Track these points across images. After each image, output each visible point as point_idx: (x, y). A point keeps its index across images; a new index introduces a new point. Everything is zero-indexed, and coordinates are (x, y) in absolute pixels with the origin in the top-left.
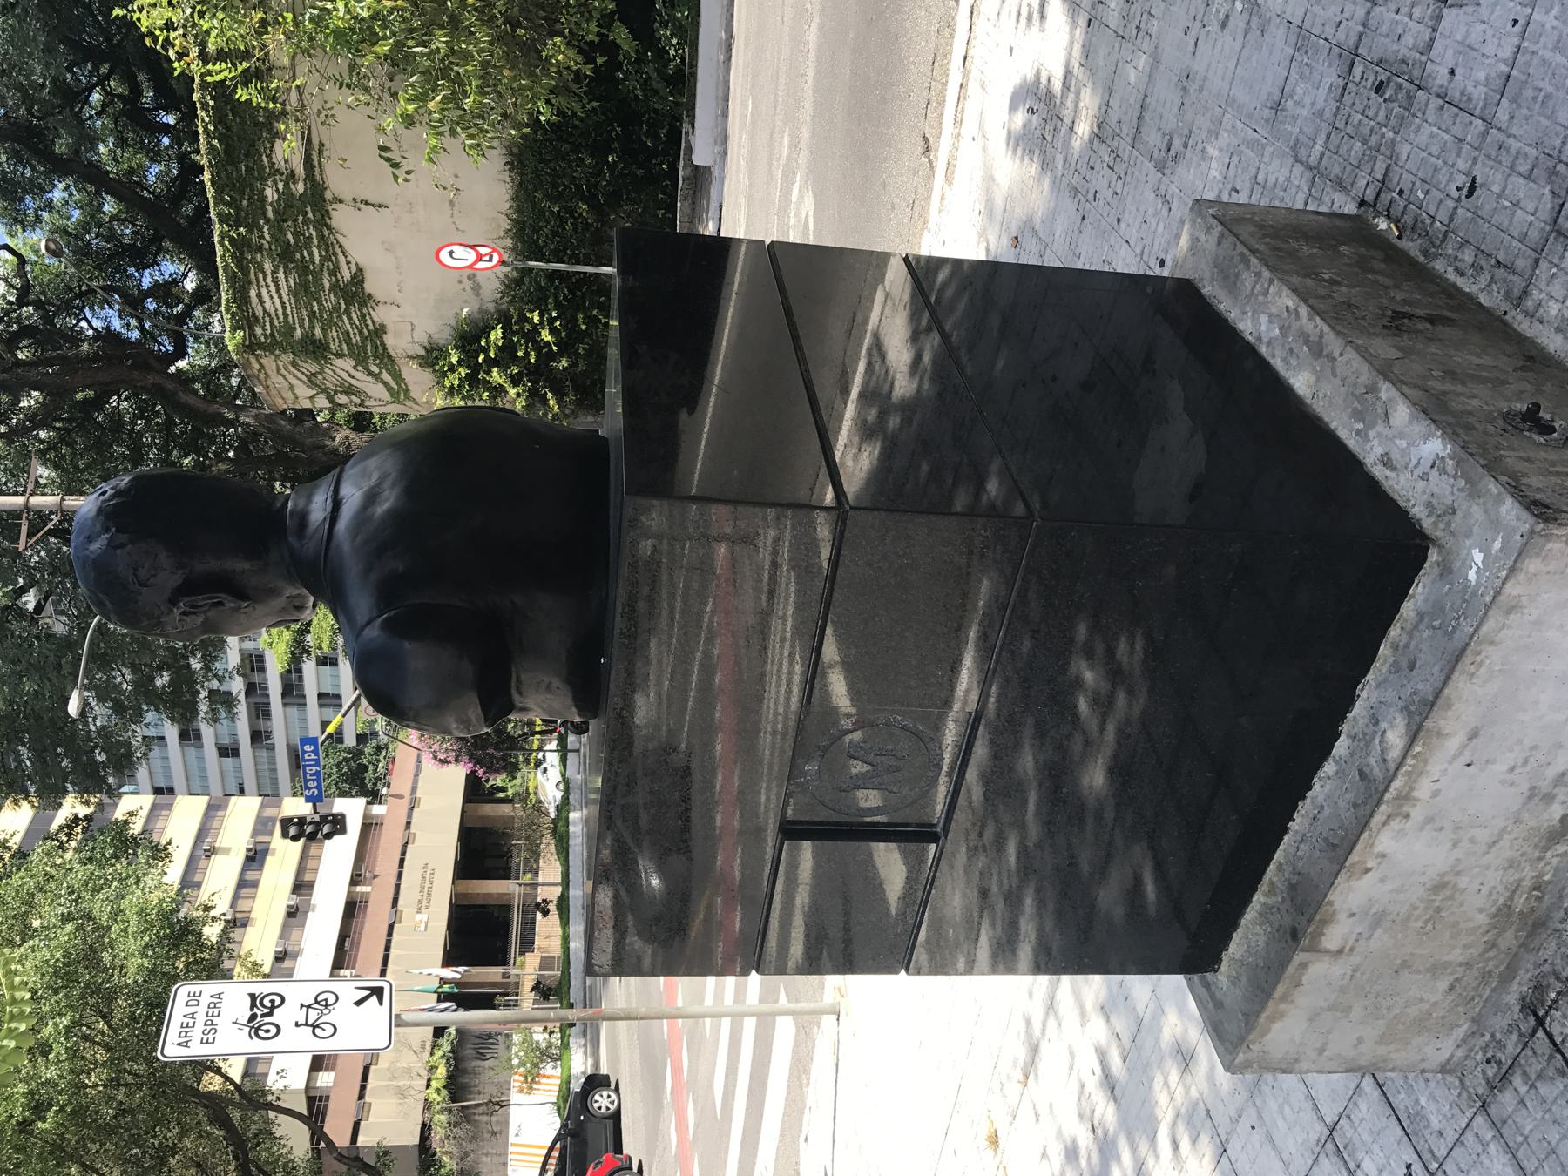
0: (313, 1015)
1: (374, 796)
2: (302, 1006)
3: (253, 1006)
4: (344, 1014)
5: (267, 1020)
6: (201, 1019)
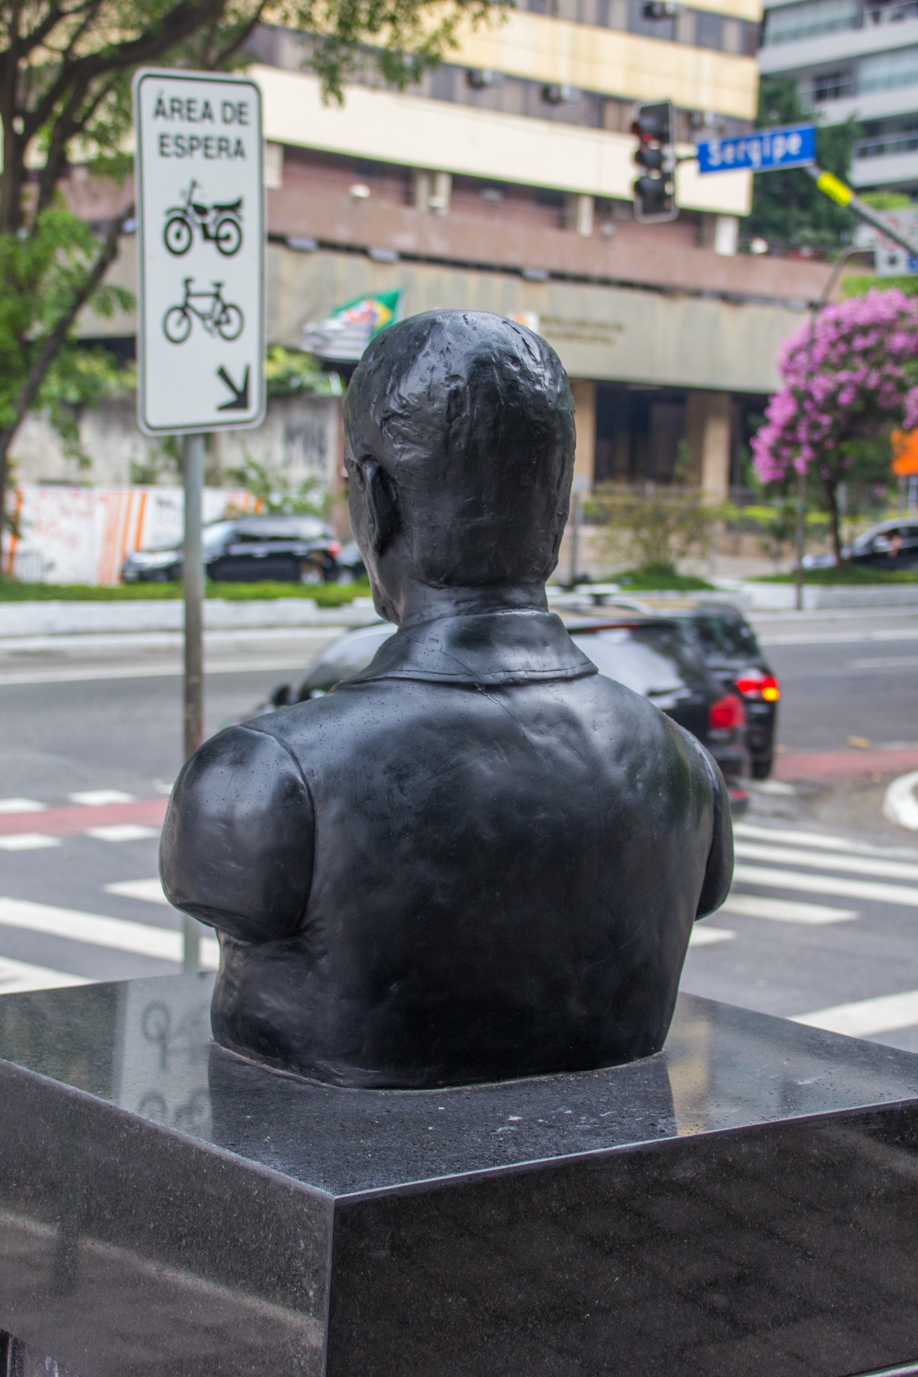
0: (203, 305)
2: (218, 285)
3: (220, 208)
5: (198, 234)
6: (202, 129)
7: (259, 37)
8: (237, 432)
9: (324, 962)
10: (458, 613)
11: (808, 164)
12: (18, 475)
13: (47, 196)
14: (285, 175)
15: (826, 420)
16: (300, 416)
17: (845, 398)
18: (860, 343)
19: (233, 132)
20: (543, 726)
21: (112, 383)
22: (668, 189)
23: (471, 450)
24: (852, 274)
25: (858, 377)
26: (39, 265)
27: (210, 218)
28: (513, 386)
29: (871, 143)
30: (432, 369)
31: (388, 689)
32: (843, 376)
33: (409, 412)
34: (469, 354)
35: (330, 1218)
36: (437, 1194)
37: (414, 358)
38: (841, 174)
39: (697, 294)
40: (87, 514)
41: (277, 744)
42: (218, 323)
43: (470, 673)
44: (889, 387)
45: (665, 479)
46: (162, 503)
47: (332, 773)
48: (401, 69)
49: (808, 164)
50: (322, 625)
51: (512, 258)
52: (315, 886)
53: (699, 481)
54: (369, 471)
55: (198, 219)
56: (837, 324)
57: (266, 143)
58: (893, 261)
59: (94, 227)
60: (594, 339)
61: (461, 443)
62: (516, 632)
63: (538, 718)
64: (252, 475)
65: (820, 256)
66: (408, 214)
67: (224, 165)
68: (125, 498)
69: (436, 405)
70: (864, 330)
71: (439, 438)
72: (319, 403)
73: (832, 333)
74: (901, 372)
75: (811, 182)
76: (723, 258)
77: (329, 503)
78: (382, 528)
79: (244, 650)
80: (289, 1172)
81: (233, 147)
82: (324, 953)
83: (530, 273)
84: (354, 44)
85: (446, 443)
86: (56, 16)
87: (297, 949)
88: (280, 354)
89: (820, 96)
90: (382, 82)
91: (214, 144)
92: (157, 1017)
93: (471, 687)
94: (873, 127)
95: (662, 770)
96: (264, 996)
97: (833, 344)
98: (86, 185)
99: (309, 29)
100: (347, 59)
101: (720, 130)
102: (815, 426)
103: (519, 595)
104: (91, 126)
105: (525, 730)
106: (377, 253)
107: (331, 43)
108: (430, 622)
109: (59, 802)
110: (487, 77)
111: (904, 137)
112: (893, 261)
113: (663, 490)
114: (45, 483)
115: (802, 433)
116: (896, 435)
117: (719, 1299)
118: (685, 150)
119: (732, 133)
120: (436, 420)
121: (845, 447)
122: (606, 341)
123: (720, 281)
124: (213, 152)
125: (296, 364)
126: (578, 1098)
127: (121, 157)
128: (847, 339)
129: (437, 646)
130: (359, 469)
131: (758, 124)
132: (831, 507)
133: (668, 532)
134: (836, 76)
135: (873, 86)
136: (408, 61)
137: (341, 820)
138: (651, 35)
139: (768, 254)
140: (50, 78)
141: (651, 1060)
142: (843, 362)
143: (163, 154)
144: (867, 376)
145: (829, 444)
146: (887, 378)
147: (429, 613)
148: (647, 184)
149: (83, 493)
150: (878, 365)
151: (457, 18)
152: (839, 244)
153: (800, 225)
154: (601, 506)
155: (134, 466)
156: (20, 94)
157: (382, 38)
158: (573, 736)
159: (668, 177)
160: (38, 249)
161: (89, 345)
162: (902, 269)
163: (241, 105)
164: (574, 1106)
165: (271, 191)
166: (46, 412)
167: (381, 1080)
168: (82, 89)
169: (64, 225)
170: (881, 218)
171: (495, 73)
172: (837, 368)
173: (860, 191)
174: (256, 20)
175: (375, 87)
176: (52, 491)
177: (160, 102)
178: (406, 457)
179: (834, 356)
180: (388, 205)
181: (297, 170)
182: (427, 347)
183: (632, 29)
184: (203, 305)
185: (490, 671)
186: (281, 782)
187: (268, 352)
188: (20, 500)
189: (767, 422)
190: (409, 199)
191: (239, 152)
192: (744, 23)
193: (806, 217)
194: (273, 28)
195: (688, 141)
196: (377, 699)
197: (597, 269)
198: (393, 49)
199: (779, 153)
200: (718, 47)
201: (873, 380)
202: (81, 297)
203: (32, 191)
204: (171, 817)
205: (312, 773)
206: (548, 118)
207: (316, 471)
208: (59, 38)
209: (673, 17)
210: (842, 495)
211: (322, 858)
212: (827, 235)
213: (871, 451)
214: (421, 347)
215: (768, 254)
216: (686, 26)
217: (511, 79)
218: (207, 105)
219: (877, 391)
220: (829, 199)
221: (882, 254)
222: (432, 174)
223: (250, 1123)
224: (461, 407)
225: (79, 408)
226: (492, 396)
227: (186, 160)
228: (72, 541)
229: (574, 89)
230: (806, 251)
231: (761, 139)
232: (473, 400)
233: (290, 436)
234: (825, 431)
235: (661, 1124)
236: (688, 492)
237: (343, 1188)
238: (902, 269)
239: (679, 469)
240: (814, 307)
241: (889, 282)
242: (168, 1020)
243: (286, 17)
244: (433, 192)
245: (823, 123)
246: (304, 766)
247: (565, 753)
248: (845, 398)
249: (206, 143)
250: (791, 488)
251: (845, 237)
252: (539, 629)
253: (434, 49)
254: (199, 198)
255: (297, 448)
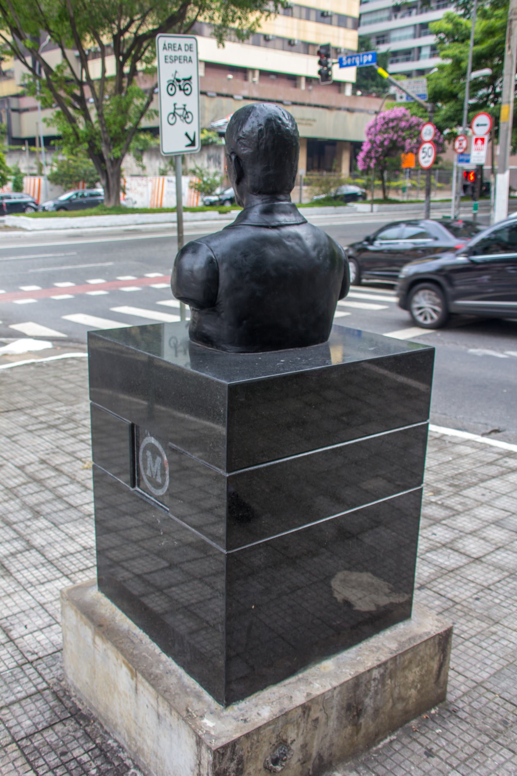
0: (180, 112)
1: (356, 87)
2: (185, 105)
3: (185, 80)
4: (181, 127)
5: (178, 88)
6: (178, 53)
7: (196, 26)
8: (192, 155)
9: (223, 315)
10: (263, 203)
11: (374, 64)
12: (124, 173)
13: (130, 81)
14: (206, 72)
15: (380, 150)
16: (212, 151)
17: (386, 143)
18: (391, 125)
19: (188, 54)
20: (290, 239)
21: (153, 143)
22: (330, 73)
23: (266, 149)
24: (388, 102)
25: (390, 136)
26: (129, 104)
27: (182, 83)
28: (279, 127)
29: (395, 59)
30: (253, 122)
31: (241, 228)
32: (386, 136)
33: (246, 137)
34: (265, 117)
35: (227, 389)
36: (259, 383)
37: (247, 119)
38: (385, 68)
39: (339, 109)
40: (146, 186)
41: (206, 246)
42: (185, 118)
43: (267, 222)
44: (400, 139)
45: (330, 170)
46: (169, 181)
47: (224, 255)
48: (243, 35)
49: (374, 64)
50: (221, 219)
51: (280, 98)
52: (219, 291)
53: (340, 171)
54: (233, 157)
55: (178, 84)
56: (384, 118)
57: (199, 61)
58: (401, 98)
59: (146, 91)
60: (306, 124)
61: (263, 147)
62: (281, 209)
63: (289, 237)
64: (198, 171)
65: (378, 96)
66: (246, 84)
67: (186, 65)
68: (158, 180)
69: (255, 134)
70: (392, 120)
71: (256, 145)
72: (218, 147)
73: (382, 122)
74: (404, 134)
75: (375, 71)
76: (347, 97)
77: (222, 179)
78: (238, 176)
79: (197, 228)
80: (214, 376)
81: (188, 59)
82: (223, 312)
83: (285, 102)
84: (227, 27)
85: (258, 147)
86: (132, 21)
87: (214, 311)
88: (205, 131)
89: (378, 43)
90: (237, 39)
91: (182, 58)
92: (173, 341)
93: (267, 227)
94: (395, 54)
95: (328, 253)
96: (204, 325)
97: (383, 125)
98: (143, 77)
99: (213, 22)
100: (225, 32)
101: (346, 54)
102: (377, 152)
103: (282, 197)
104: (143, 58)
105: (285, 241)
106: (236, 97)
107: (220, 27)
108: (254, 206)
109: (141, 277)
110: (271, 37)
111: (405, 57)
112: (401, 98)
113: (329, 174)
114: (132, 176)
115: (373, 154)
116: (403, 155)
117: (345, 419)
118: (335, 61)
119: (350, 54)
120: (254, 140)
121: (387, 159)
122: (310, 125)
123: (346, 105)
124: (182, 61)
125: (211, 134)
126: (302, 355)
127: (153, 67)
128: (387, 123)
129: (256, 214)
130: (230, 157)
131: (358, 51)
132: (382, 178)
133: (331, 187)
134: (383, 36)
135: (395, 40)
136: (245, 32)
137: (227, 270)
138: (323, 22)
139: (362, 95)
140: (130, 43)
141: (324, 344)
142: (386, 131)
143: (166, 62)
144: (393, 136)
145: (382, 158)
146: (399, 136)
147: (253, 204)
148: (323, 71)
149: (145, 178)
150: (397, 132)
151: (261, 17)
152: (384, 92)
153: (372, 86)
154: (309, 179)
155: (160, 169)
156: (121, 49)
157: (236, 25)
158: (300, 242)
159: (329, 69)
160: (128, 100)
161: (145, 130)
162: (404, 100)
163: (191, 45)
164: (301, 357)
165: (201, 77)
166: (132, 153)
167: (242, 350)
168: (141, 46)
169: (135, 91)
170: (398, 83)
171: (273, 36)
172: (384, 133)
173: (391, 74)
174: (195, 20)
175: (234, 41)
176: (134, 178)
177: (165, 45)
178: (245, 152)
179: (383, 129)
180: (239, 81)
181: (210, 70)
182: (251, 115)
183: (317, 21)
184: (180, 112)
185: (273, 222)
186: (208, 258)
187: (202, 131)
188: (125, 182)
189: (362, 150)
190: (246, 79)
191: (190, 61)
192: (353, 19)
193: (374, 83)
194: (201, 23)
195: (336, 58)
196: (237, 231)
197: (307, 101)
198: (240, 28)
199: (365, 61)
200: (345, 27)
201: (395, 137)
202: (142, 114)
203: (126, 80)
204: (174, 270)
205: (217, 255)
206: (290, 51)
207: (218, 170)
208: (133, 29)
209: (331, 16)
210: (386, 175)
211: (221, 282)
212: (380, 89)
213: (394, 160)
214: (249, 115)
215: (362, 95)
216: (335, 19)
217: (278, 38)
218: (180, 45)
219: (396, 140)
220: (381, 77)
221: (398, 96)
222: (253, 70)
223: (202, 363)
224: (263, 135)
225: (142, 152)
226: (272, 131)
227: (174, 64)
228: (142, 194)
229: (298, 41)
230: (374, 95)
231: (359, 56)
232: (266, 133)
233: (209, 158)
234: (380, 153)
235: (327, 362)
236: (337, 174)
237: (230, 381)
238: (404, 100)
239: (334, 167)
240: (377, 113)
241: (400, 104)
242: (177, 341)
243: (205, 19)
244: (254, 76)
245: (379, 52)
246: (215, 253)
247: (297, 248)
248: (386, 143)
249: (179, 58)
250: (370, 172)
251: (386, 90)
252: (289, 208)
253: (253, 28)
254: (178, 77)
255: (212, 162)
